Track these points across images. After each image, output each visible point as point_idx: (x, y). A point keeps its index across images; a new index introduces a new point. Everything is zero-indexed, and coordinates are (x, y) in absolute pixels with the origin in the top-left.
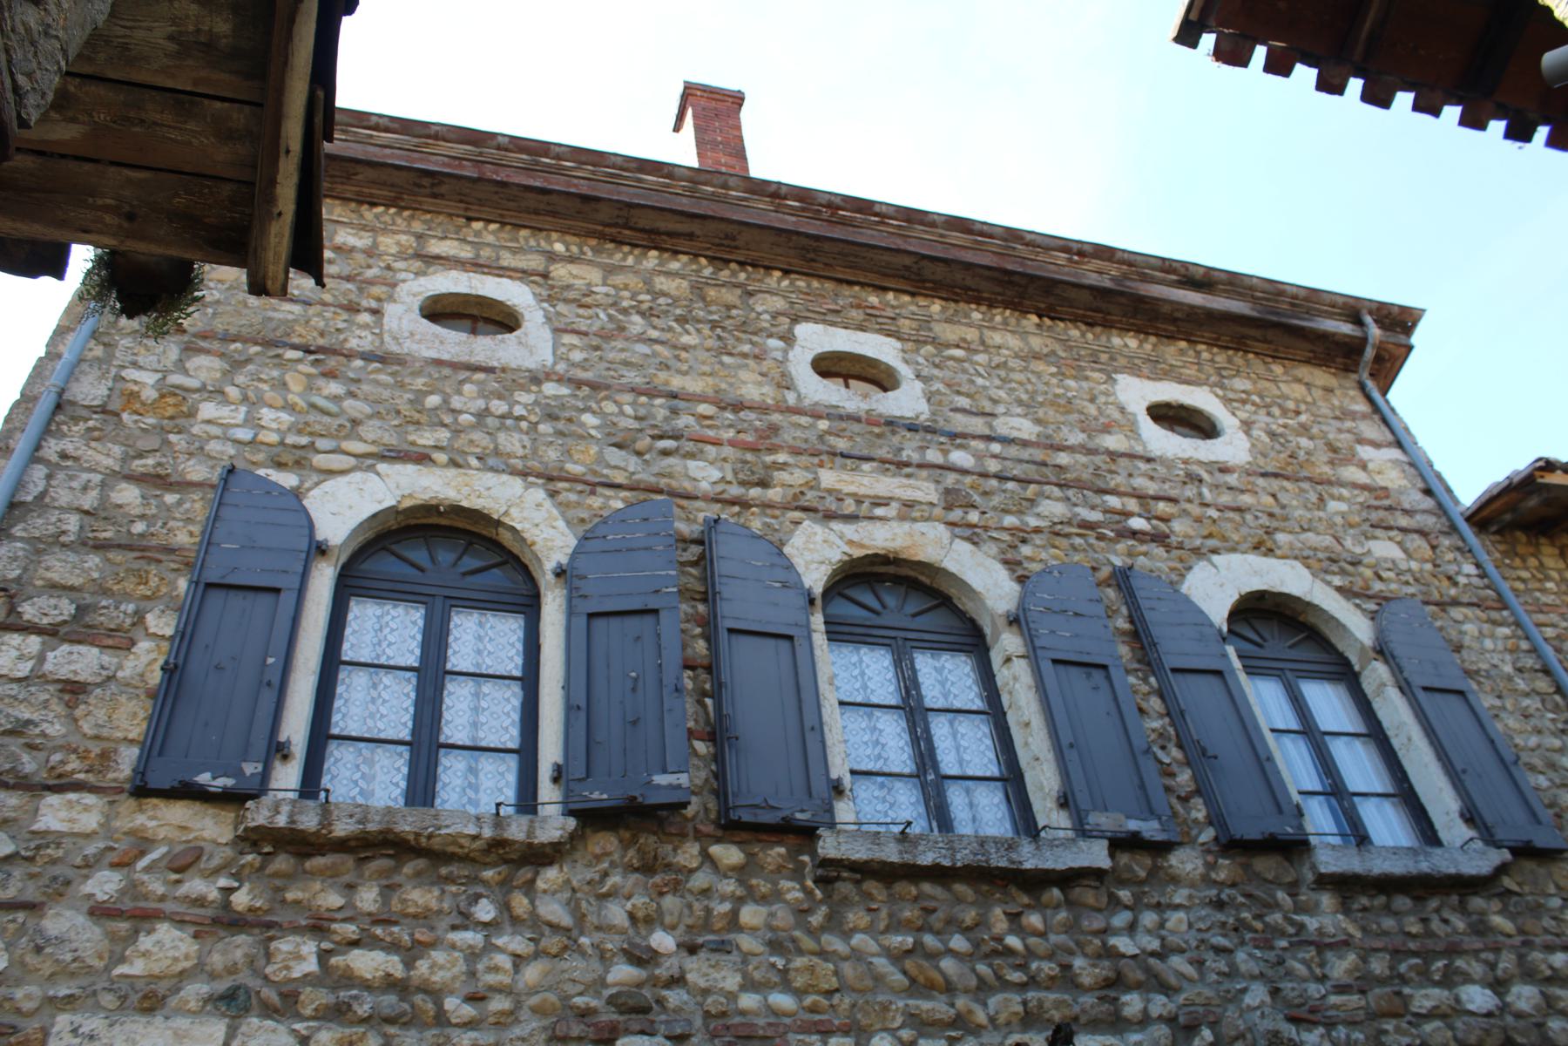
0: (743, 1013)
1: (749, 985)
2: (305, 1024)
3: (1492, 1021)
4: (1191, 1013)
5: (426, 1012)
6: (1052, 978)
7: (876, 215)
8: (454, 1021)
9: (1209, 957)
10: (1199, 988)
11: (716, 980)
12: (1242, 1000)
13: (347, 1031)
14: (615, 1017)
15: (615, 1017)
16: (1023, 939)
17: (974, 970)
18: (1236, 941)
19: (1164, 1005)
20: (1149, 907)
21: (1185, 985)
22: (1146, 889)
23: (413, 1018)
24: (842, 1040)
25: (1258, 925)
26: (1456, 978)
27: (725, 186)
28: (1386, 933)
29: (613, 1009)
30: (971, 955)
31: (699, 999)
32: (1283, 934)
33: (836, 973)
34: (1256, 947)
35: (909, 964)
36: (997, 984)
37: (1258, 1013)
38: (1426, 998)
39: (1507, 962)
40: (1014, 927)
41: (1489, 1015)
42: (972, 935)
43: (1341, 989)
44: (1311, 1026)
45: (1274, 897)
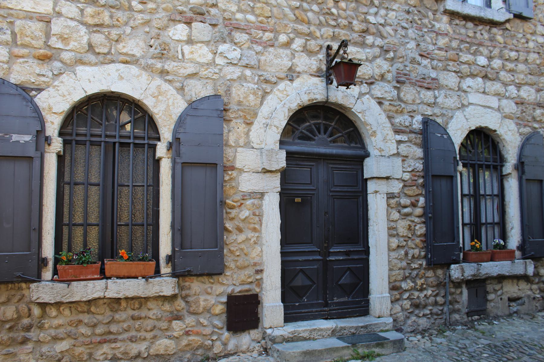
0: (237, 20)
1: (240, 10)
2: (82, 5)
3: (484, 69)
4: (389, 46)
5: (125, 5)
6: (345, 26)
8: (135, 10)
9: (400, 29)
10: (393, 39)
11: (228, 7)
12: (406, 46)
13: (97, 9)
14: (192, 15)
15: (192, 15)
16: (338, 11)
17: (319, 18)
18: (410, 26)
19: (380, 42)
20: (384, 8)
21: (389, 37)
22: (384, 2)
23: (120, 7)
24: (269, 34)
25: (419, 22)
26: (478, 53)
28: (461, 34)
29: (192, 12)
30: (318, 13)
31: (222, 13)
32: (427, 27)
33: (271, 11)
34: (416, 29)
35: (297, 12)
36: (326, 24)
37: (411, 51)
38: (465, 57)
39: (496, 52)
40: (335, 6)
41: (483, 67)
42: (320, 6)
43: (440, 49)
44: (426, 58)
45: (427, 13)
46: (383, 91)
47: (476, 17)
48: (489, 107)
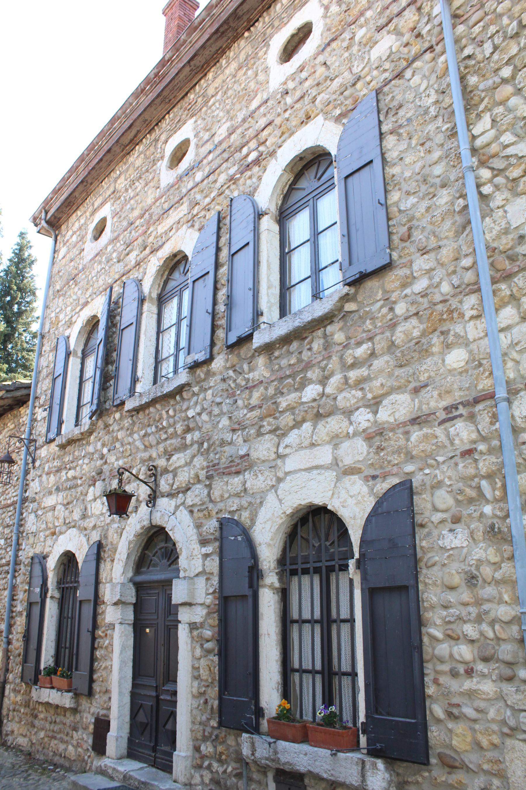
7: (168, 61)
27: (131, 104)
46: (193, 497)
47: (291, 332)
48: (317, 467)
